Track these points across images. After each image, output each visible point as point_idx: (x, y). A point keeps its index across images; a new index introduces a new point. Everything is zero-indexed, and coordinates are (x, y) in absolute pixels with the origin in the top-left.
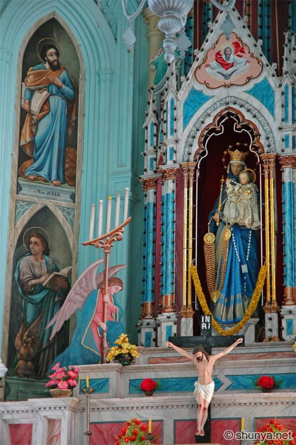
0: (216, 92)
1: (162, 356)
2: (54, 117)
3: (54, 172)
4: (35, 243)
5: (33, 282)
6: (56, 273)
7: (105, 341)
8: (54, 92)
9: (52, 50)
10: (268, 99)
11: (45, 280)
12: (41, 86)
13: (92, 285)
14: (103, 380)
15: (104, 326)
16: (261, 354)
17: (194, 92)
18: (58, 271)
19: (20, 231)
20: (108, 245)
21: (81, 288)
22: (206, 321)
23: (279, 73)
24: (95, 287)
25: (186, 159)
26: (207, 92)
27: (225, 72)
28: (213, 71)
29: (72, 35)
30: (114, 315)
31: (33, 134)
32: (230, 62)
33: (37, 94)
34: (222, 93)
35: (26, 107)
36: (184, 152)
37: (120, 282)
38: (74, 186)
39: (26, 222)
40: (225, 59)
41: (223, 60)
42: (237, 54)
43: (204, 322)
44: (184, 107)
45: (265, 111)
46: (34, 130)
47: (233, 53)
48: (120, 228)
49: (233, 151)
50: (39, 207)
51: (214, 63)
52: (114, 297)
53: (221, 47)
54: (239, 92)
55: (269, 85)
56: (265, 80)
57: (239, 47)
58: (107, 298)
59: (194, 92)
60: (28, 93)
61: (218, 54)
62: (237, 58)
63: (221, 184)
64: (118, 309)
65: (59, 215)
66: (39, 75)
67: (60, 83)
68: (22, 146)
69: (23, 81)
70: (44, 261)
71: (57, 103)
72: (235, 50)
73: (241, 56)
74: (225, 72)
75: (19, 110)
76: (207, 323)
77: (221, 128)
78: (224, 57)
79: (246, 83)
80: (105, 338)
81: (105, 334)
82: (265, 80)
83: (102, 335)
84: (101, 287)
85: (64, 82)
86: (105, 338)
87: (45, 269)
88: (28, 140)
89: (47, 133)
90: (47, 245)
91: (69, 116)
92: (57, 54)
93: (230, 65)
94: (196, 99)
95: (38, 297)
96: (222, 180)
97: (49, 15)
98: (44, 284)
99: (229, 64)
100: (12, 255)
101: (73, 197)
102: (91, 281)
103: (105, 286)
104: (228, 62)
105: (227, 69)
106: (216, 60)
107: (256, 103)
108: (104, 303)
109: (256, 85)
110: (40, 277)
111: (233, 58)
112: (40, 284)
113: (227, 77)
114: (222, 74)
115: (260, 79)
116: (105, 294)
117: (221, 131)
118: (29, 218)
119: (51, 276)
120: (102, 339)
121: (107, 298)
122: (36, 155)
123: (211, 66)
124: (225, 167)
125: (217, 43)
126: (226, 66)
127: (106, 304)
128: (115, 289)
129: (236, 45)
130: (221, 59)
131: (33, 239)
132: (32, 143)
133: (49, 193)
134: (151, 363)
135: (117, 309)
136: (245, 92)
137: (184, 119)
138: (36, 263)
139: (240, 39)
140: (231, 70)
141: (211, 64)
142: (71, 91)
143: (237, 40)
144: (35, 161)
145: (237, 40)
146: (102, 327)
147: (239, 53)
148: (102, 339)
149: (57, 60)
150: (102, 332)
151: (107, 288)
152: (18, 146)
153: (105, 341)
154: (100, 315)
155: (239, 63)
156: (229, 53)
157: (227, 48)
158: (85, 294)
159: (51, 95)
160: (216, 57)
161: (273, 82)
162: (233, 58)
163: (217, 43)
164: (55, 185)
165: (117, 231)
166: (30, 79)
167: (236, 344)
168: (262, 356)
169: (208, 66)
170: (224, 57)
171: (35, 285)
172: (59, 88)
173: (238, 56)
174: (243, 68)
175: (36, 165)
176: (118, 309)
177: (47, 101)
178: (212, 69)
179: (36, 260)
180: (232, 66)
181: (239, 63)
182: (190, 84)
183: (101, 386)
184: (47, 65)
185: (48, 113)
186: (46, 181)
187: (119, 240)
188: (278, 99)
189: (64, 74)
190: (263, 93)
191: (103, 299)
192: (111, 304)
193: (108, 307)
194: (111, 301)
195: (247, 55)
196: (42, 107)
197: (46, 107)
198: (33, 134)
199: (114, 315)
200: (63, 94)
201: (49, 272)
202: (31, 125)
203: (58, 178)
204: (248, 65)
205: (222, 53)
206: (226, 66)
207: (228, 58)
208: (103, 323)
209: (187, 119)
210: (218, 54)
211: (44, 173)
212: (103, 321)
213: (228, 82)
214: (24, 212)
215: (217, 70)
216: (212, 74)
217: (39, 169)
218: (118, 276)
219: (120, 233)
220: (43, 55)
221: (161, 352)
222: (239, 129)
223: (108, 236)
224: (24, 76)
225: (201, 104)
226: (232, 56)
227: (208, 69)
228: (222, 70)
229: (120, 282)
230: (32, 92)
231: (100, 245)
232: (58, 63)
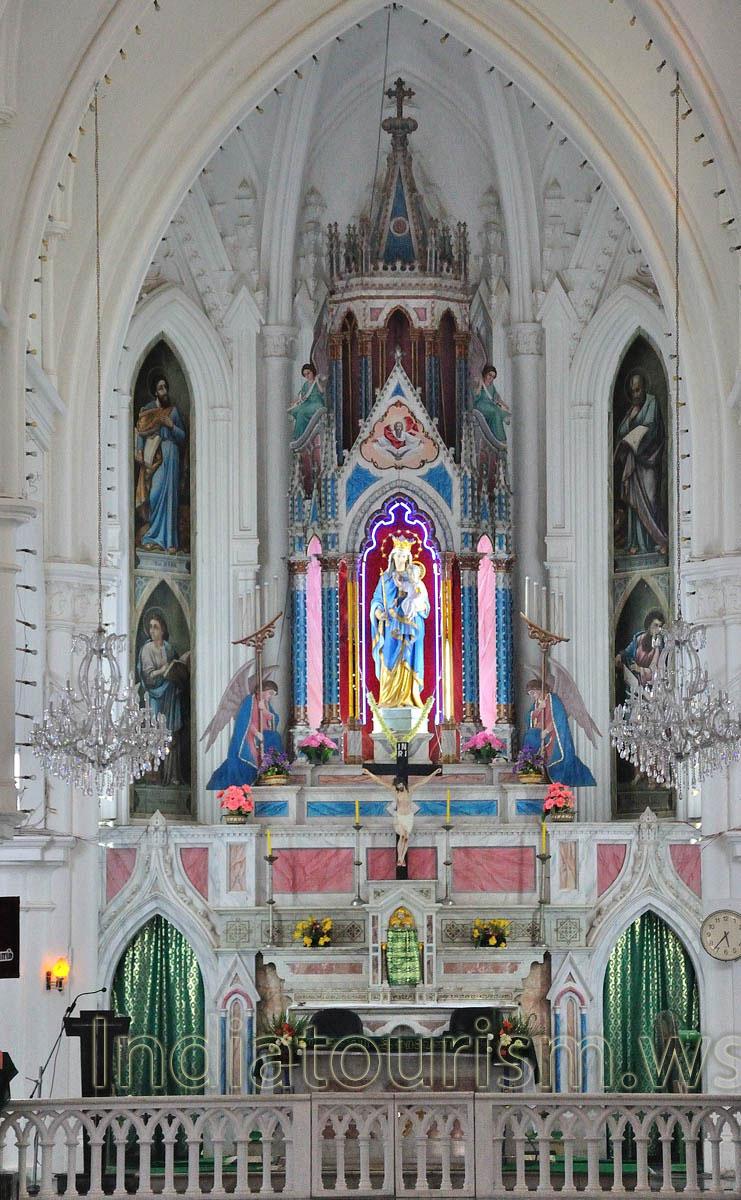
0: (384, 473)
2: (167, 466)
3: (169, 537)
4: (155, 626)
5: (155, 673)
6: (175, 661)
8: (166, 436)
9: (162, 383)
11: (165, 670)
12: (153, 430)
13: (245, 692)
15: (261, 736)
17: (358, 470)
18: (178, 658)
19: (140, 613)
21: (233, 693)
23: (457, 459)
24: (249, 693)
25: (350, 548)
26: (374, 471)
27: (395, 451)
28: (380, 448)
29: (181, 359)
31: (148, 493)
32: (402, 439)
33: (149, 441)
34: (390, 475)
35: (140, 458)
36: (348, 540)
37: (274, 686)
38: (189, 552)
39: (145, 601)
44: (347, 486)
45: (441, 501)
46: (148, 487)
48: (272, 624)
50: (156, 583)
51: (382, 439)
52: (268, 703)
53: (391, 421)
54: (413, 477)
55: (446, 473)
56: (441, 466)
57: (412, 423)
58: (262, 704)
59: (358, 470)
60: (141, 440)
61: (388, 428)
65: (176, 589)
66: (150, 416)
67: (171, 424)
68: (139, 507)
69: (135, 425)
70: (163, 648)
71: (169, 448)
73: (414, 435)
74: (395, 451)
75: (133, 461)
78: (394, 433)
79: (421, 467)
81: (262, 745)
82: (441, 466)
84: (255, 691)
85: (175, 423)
87: (165, 658)
88: (143, 500)
89: (160, 492)
90: (166, 627)
91: (181, 466)
92: (167, 386)
94: (361, 480)
95: (159, 691)
97: (157, 337)
98: (165, 675)
99: (400, 442)
100: (134, 643)
101: (188, 566)
102: (244, 684)
107: (430, 491)
108: (259, 710)
109: (431, 470)
110: (161, 666)
111: (404, 435)
112: (161, 675)
113: (398, 457)
114: (393, 454)
115: (436, 464)
118: (149, 594)
119: (172, 664)
120: (259, 750)
121: (262, 704)
122: (151, 518)
124: (384, 555)
125: (386, 415)
126: (398, 444)
128: (268, 694)
129: (409, 420)
131: (153, 622)
132: (147, 504)
133: (165, 565)
137: (348, 500)
138: (157, 651)
139: (412, 414)
140: (402, 449)
142: (182, 432)
143: (409, 415)
144: (150, 526)
145: (409, 415)
147: (412, 431)
148: (259, 750)
149: (167, 395)
150: (259, 742)
152: (133, 510)
154: (256, 724)
157: (397, 423)
158: (239, 701)
159: (163, 439)
161: (449, 468)
162: (404, 435)
163: (386, 415)
164: (171, 554)
165: (269, 626)
166: (142, 422)
167: (435, 773)
169: (376, 441)
170: (394, 433)
171: (157, 677)
172: (170, 429)
175: (152, 530)
177: (159, 450)
179: (157, 646)
182: (355, 459)
184: (157, 402)
185: (160, 465)
186: (162, 549)
187: (271, 637)
188: (456, 483)
189: (174, 411)
190: (438, 479)
192: (268, 712)
195: (420, 434)
196: (155, 457)
197: (158, 457)
198: (148, 493)
200: (174, 437)
201: (169, 661)
202: (145, 481)
203: (173, 545)
204: (422, 445)
205: (392, 428)
206: (398, 444)
207: (399, 435)
209: (350, 501)
210: (388, 428)
211: (159, 540)
213: (399, 463)
214: (142, 590)
217: (155, 536)
218: (271, 679)
219: (272, 629)
220: (154, 389)
223: (260, 632)
224: (136, 419)
225: (366, 486)
227: (375, 445)
228: (392, 448)
229: (274, 686)
230: (144, 439)
231: (253, 643)
232: (168, 399)
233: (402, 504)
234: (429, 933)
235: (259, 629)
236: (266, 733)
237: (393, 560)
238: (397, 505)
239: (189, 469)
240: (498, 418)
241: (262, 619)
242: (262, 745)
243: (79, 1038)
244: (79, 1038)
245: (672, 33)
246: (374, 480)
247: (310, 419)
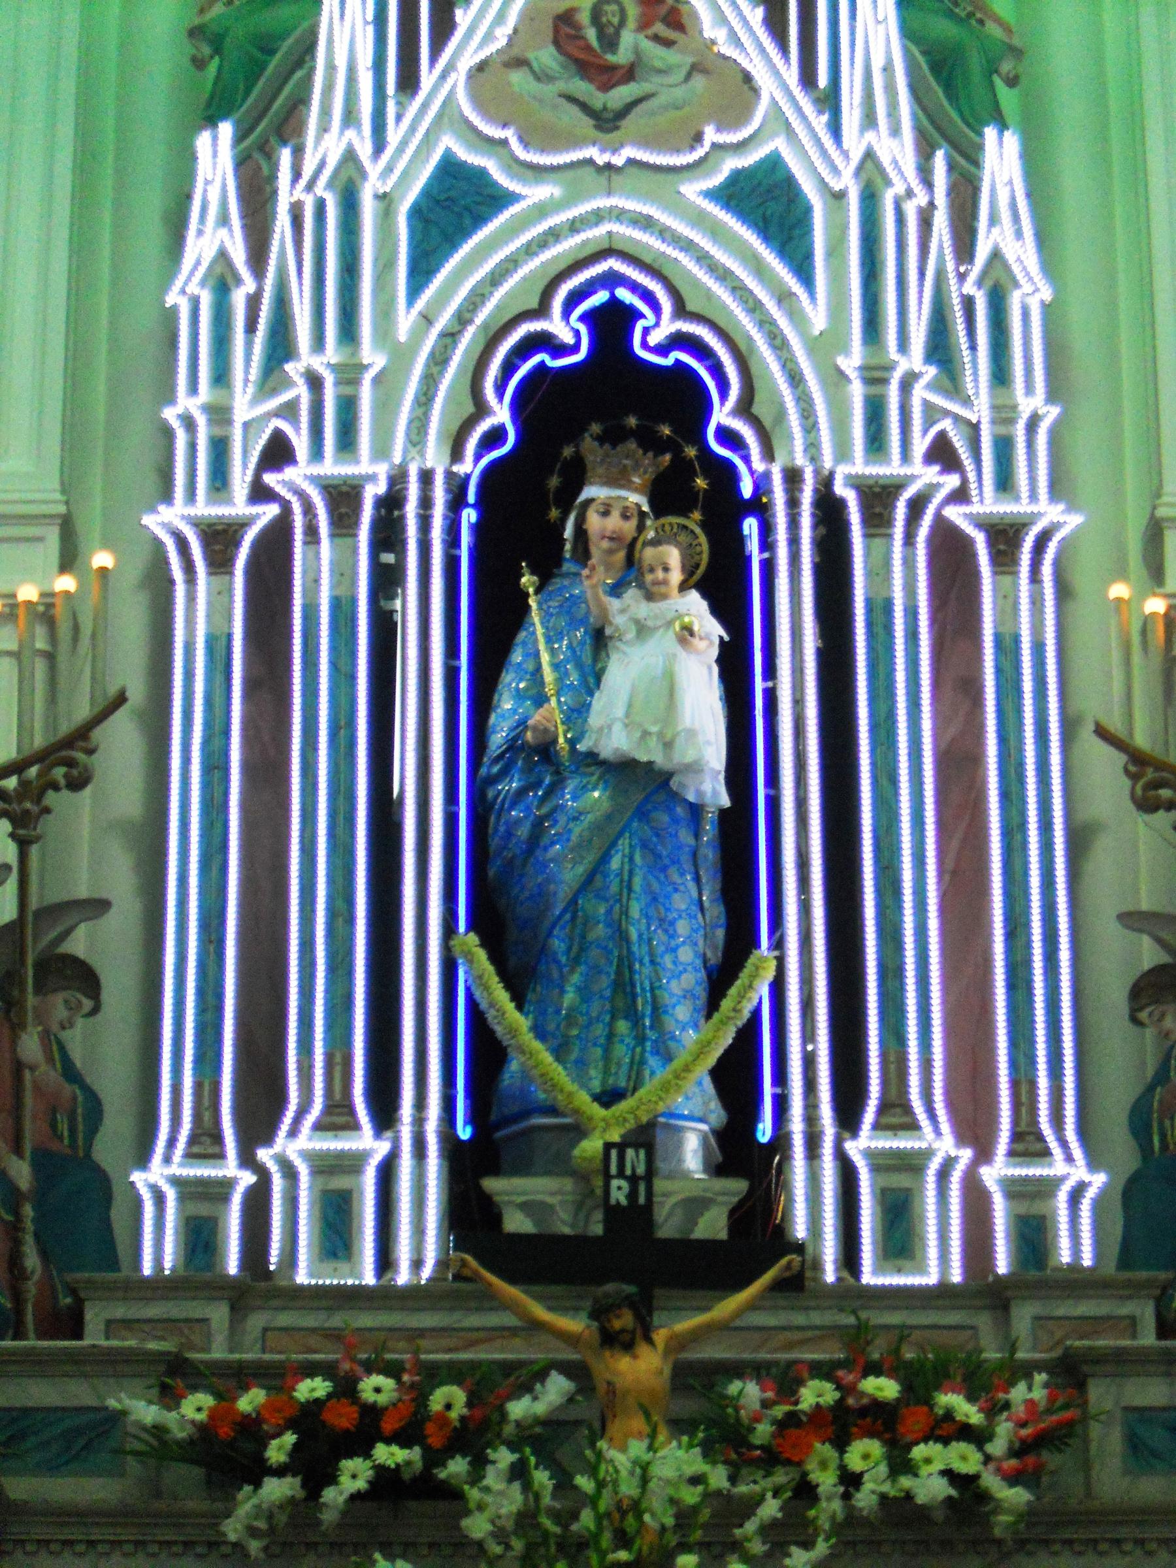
1: (327, 1325)
7: (29, 1240)
10: (790, 238)
14: (92, 1416)
15: (22, 1172)
16: (798, 1335)
20: (28, 805)
22: (628, 1172)
27: (598, 99)
30: (64, 1127)
32: (622, 57)
40: (594, 43)
41: (588, 48)
42: (650, 32)
43: (621, 1174)
47: (631, 23)
49: (614, 446)
62: (647, 45)
63: (527, 595)
64: (80, 1099)
72: (644, 14)
73: (668, 43)
76: (633, 1180)
77: (577, 333)
78: (591, 34)
80: (29, 1225)
81: (28, 1211)
83: (16, 1212)
86: (29, 1225)
93: (620, 72)
96: (524, 580)
99: (613, 68)
103: (23, 991)
104: (611, 58)
105: (605, 87)
106: (556, 43)
108: (18, 1067)
114: (585, 107)
116: (22, 1026)
117: (575, 349)
121: (30, 1045)
123: (535, 65)
124: (554, 513)
127: (27, 1075)
130: (582, 43)
134: (271, 1351)
135: (75, 1098)
136: (200, 256)
140: (623, 93)
141: (531, 56)
146: (12, 1173)
147: (659, 28)
151: (31, 1000)
153: (29, 1240)
155: (660, 71)
156: (615, 21)
160: (556, 30)
168: (809, 1340)
170: (591, 34)
173: (656, 38)
174: (679, 93)
176: (80, 1099)
178: (538, 79)
180: (629, 74)
181: (660, 71)
183: (81, 1442)
191: (14, 1051)
192: (51, 1076)
193: (37, 1088)
194: (50, 1060)
199: (64, 1127)
205: (584, 18)
207: (610, 42)
208: (14, 1158)
212: (18, 1150)
215: (561, 86)
216: (541, 101)
219: (80, 756)
221: (324, 1303)
222: (662, 350)
226: (628, 38)
228: (582, 87)
233: (623, 294)
234: (219, 396)
235: (39, 741)
236: (43, 1162)
237: (581, 533)
238: (600, 298)
239: (440, 1309)
240: (975, 63)
241: (51, 718)
242: (28, 1211)
243: (723, 1235)
244: (723, 1235)
245: (960, 320)
246: (513, 198)
247: (272, 52)
